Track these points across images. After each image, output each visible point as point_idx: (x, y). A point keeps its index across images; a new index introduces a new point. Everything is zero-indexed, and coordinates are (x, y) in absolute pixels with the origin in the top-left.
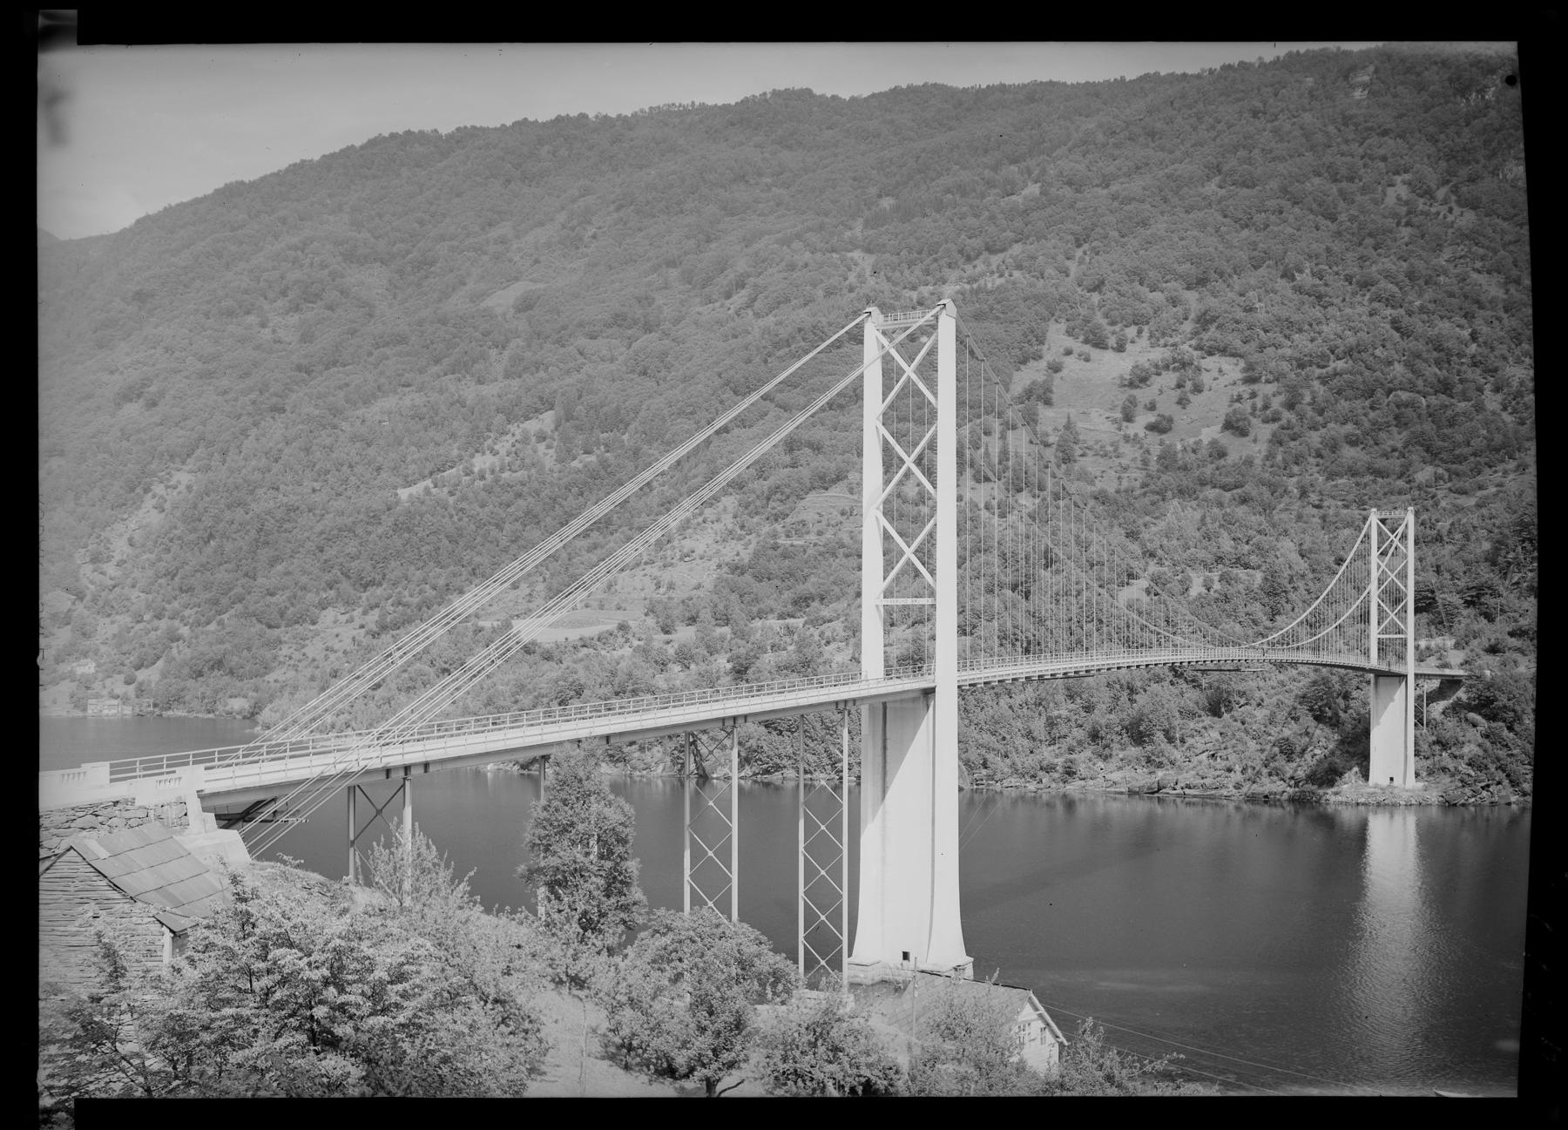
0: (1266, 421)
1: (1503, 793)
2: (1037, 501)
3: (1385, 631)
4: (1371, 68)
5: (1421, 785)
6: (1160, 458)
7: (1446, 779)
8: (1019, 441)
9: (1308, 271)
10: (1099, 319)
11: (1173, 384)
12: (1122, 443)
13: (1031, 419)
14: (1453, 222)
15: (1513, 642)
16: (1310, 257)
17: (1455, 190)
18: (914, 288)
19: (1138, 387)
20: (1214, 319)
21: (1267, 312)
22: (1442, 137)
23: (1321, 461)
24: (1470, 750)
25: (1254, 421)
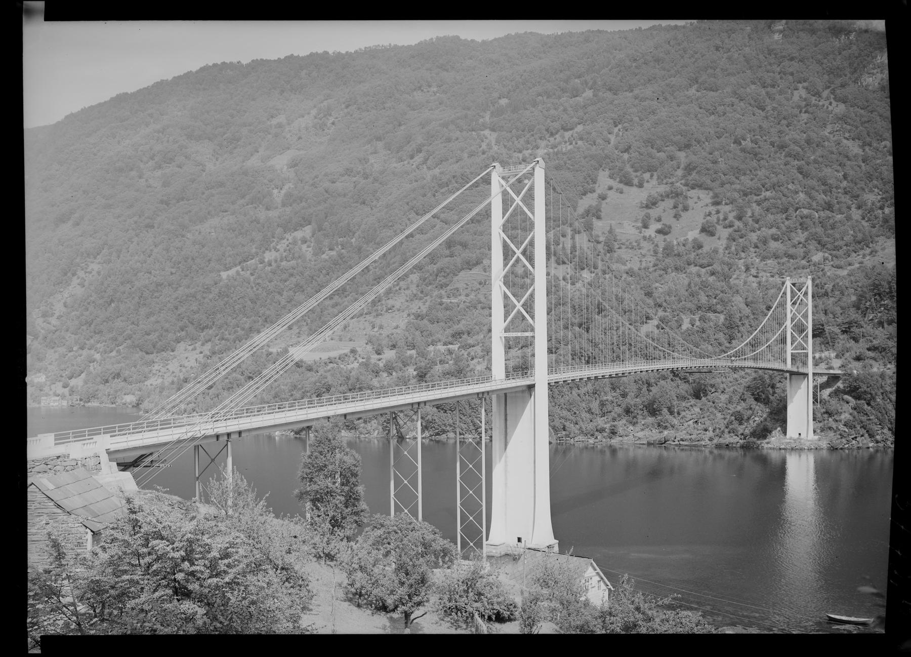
0: (725, 227)
1: (865, 442)
2: (593, 275)
3: (795, 348)
5: (816, 437)
6: (664, 249)
7: (831, 434)
8: (582, 240)
9: (749, 139)
10: (628, 169)
11: (671, 206)
12: (642, 241)
13: (589, 228)
15: (871, 354)
17: (833, 92)
18: (520, 152)
19: (651, 208)
20: (695, 168)
22: (825, 61)
23: (757, 250)
24: (845, 416)
25: (719, 227)
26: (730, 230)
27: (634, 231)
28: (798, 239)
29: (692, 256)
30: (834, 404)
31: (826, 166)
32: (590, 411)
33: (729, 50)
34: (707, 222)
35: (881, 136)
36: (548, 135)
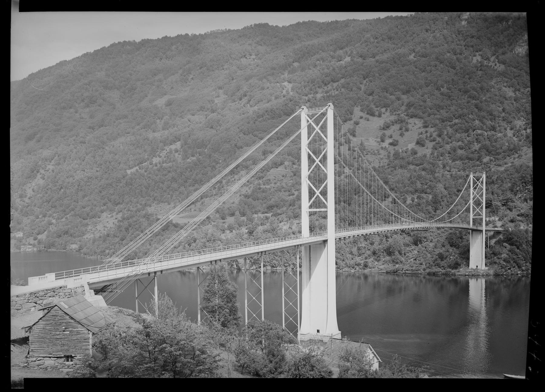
0: (431, 141)
3: (475, 216)
5: (487, 268)
6: (394, 155)
9: (445, 87)
11: (398, 128)
12: (380, 150)
14: (496, 69)
15: (519, 218)
17: (497, 57)
23: (450, 155)
24: (504, 256)
25: (427, 141)
26: (434, 143)
28: (474, 148)
30: (498, 248)
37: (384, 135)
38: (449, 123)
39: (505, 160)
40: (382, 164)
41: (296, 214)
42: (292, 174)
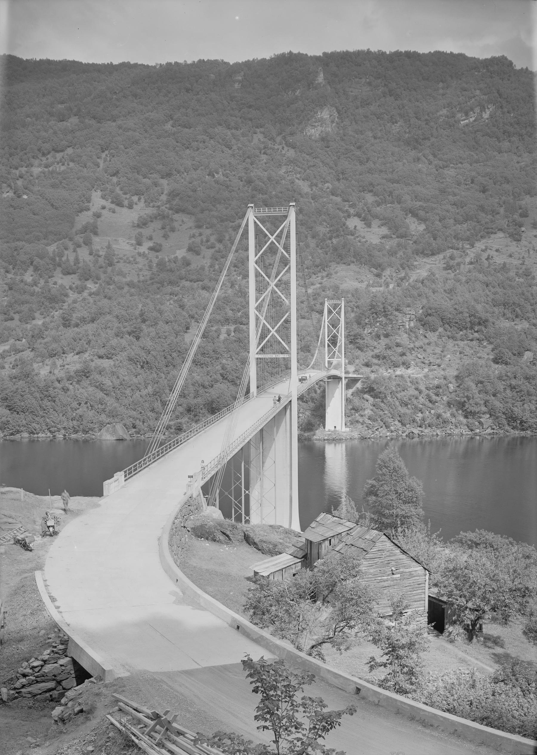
0: (208, 248)
1: (384, 432)
2: (97, 285)
3: (329, 358)
4: (242, 73)
5: (348, 429)
6: (158, 265)
7: (360, 426)
8: (83, 254)
9: (221, 173)
10: (118, 190)
11: (160, 226)
12: (137, 256)
13: (88, 243)
14: (285, 154)
15: (375, 361)
16: (222, 166)
17: (284, 138)
18: (17, 168)
19: (142, 227)
20: (178, 195)
21: (204, 193)
22: (277, 111)
23: (237, 269)
24: (368, 412)
25: (202, 247)
26: (213, 250)
27: (128, 247)
28: (268, 261)
29: (183, 272)
30: (357, 402)
31: (285, 201)
32: (153, 410)
33: (198, 94)
34: (193, 242)
35: (324, 179)
36: (41, 155)
37: (140, 234)
38: (231, 224)
39: (311, 280)
40: (142, 278)
41: (53, 350)
42: (6, 288)
